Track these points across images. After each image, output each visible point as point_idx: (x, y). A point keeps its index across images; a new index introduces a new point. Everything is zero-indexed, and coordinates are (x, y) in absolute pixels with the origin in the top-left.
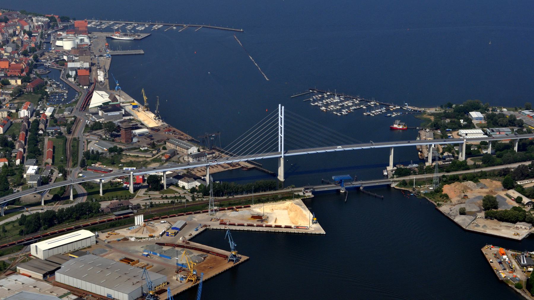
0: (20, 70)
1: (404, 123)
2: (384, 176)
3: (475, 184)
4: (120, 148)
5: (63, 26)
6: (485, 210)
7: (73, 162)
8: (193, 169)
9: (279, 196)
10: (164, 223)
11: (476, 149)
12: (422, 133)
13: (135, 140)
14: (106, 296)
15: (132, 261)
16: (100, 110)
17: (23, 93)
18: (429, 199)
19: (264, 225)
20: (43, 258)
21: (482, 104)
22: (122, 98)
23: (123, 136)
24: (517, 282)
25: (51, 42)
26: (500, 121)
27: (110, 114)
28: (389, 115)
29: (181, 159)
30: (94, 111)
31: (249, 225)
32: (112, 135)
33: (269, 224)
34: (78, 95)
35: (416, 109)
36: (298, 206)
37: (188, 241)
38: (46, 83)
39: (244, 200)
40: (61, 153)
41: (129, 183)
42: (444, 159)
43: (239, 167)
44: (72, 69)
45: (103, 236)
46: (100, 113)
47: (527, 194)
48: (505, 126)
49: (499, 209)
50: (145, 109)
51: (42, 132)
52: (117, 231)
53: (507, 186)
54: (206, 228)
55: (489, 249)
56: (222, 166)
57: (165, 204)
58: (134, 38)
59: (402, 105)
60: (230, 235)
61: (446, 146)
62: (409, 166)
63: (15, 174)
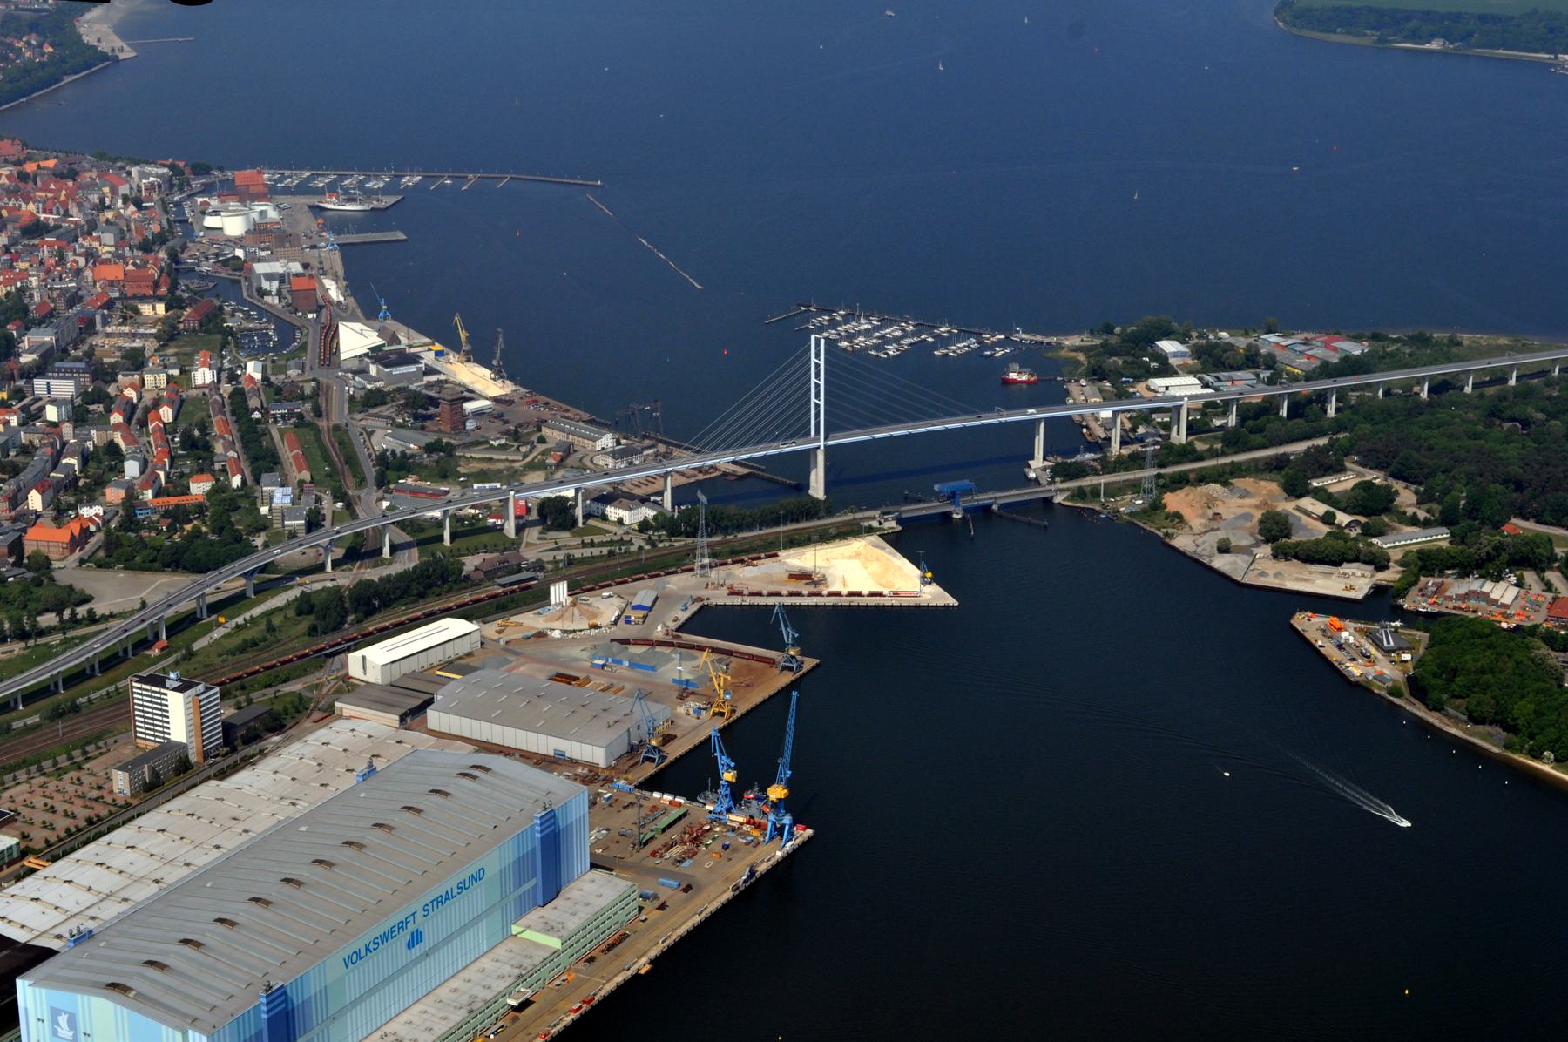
0: (151, 283)
1: (1029, 370)
2: (1030, 480)
3: (1227, 490)
4: (448, 444)
5: (203, 184)
6: (1267, 541)
7: (354, 476)
8: (622, 483)
9: (832, 531)
10: (610, 596)
11: (1198, 417)
12: (1073, 388)
13: (470, 425)
14: (552, 754)
15: (576, 679)
16: (373, 363)
17: (179, 333)
18: (1142, 525)
19: (825, 592)
20: (379, 677)
21: (1176, 325)
22: (408, 339)
23: (446, 416)
24: (1390, 684)
25: (190, 220)
26: (1228, 358)
27: (396, 371)
28: (988, 353)
29: (587, 461)
30: (355, 365)
31: (791, 594)
32: (416, 417)
33: (834, 589)
34: (301, 333)
35: (1039, 338)
36: (879, 551)
37: (675, 633)
38: (221, 309)
39: (759, 543)
40: (319, 458)
41: (505, 517)
42: (1140, 440)
43: (717, 473)
44: (270, 277)
45: (491, 630)
46: (373, 370)
47: (1343, 505)
48: (1240, 369)
49: (1294, 539)
50: (464, 359)
51: (260, 416)
52: (515, 619)
53: (1295, 489)
54: (701, 604)
55: (1305, 620)
56: (682, 474)
57: (593, 557)
58: (371, 206)
59: (1009, 331)
60: (782, 615)
61: (1134, 414)
62: (1078, 458)
63: (240, 507)
